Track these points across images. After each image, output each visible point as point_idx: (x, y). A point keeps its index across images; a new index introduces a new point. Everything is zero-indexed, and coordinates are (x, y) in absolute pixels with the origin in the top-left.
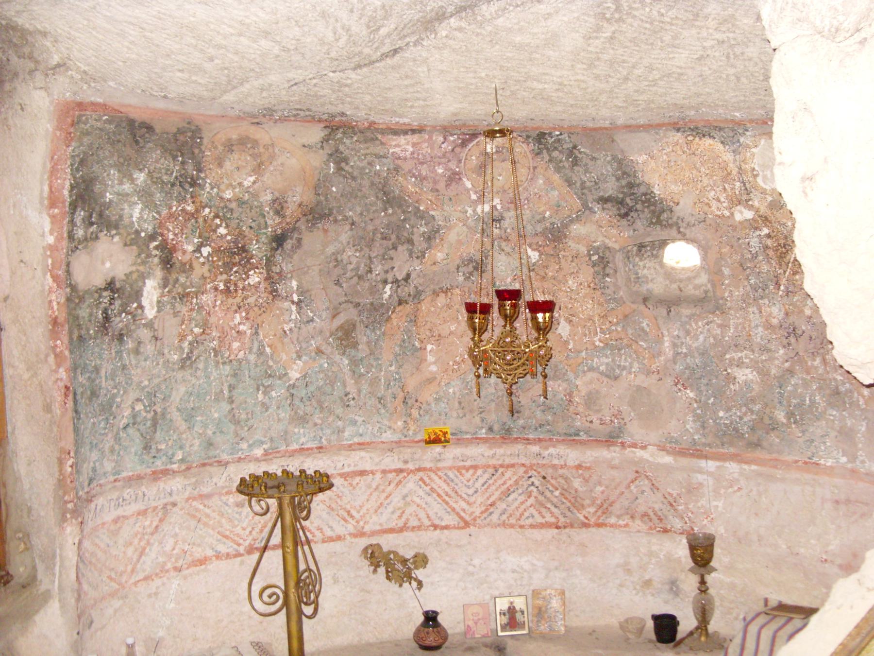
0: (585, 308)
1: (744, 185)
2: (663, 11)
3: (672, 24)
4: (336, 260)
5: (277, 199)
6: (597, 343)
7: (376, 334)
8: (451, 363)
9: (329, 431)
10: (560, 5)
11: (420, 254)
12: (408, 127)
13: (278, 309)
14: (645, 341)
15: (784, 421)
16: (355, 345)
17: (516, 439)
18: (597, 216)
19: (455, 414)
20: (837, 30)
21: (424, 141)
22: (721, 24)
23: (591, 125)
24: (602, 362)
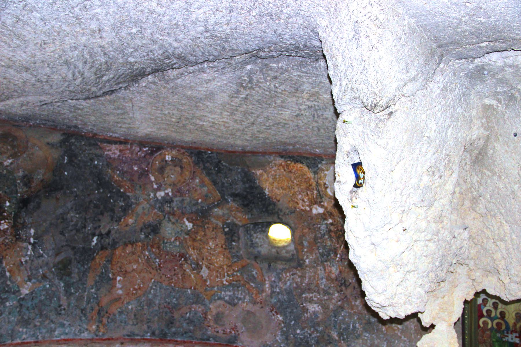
0: (218, 260)
1: (319, 193)
2: (277, 85)
3: (282, 94)
4: (63, 218)
5: (26, 175)
6: (225, 282)
7: (84, 267)
8: (132, 289)
9: (44, 331)
10: (216, 75)
11: (118, 219)
12: (118, 140)
13: (19, 247)
14: (254, 283)
15: (337, 338)
16: (69, 274)
17: (169, 340)
18: (230, 204)
19: (131, 323)
20: (376, 106)
21: (127, 149)
22: (310, 96)
23: (230, 149)
24: (227, 294)
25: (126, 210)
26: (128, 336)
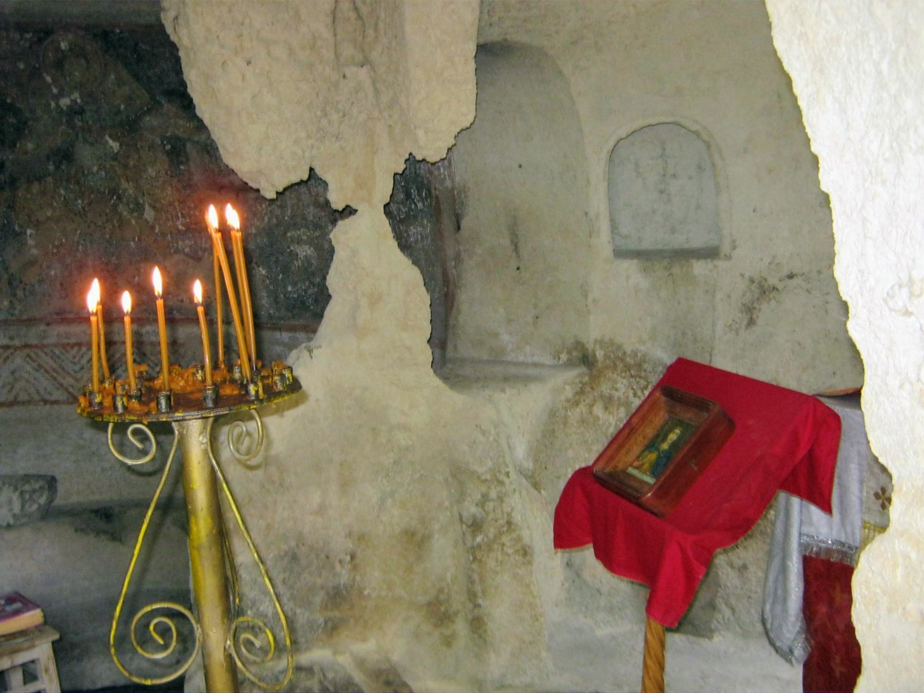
6: (180, 227)
25: (21, 129)
26: (57, 314)
